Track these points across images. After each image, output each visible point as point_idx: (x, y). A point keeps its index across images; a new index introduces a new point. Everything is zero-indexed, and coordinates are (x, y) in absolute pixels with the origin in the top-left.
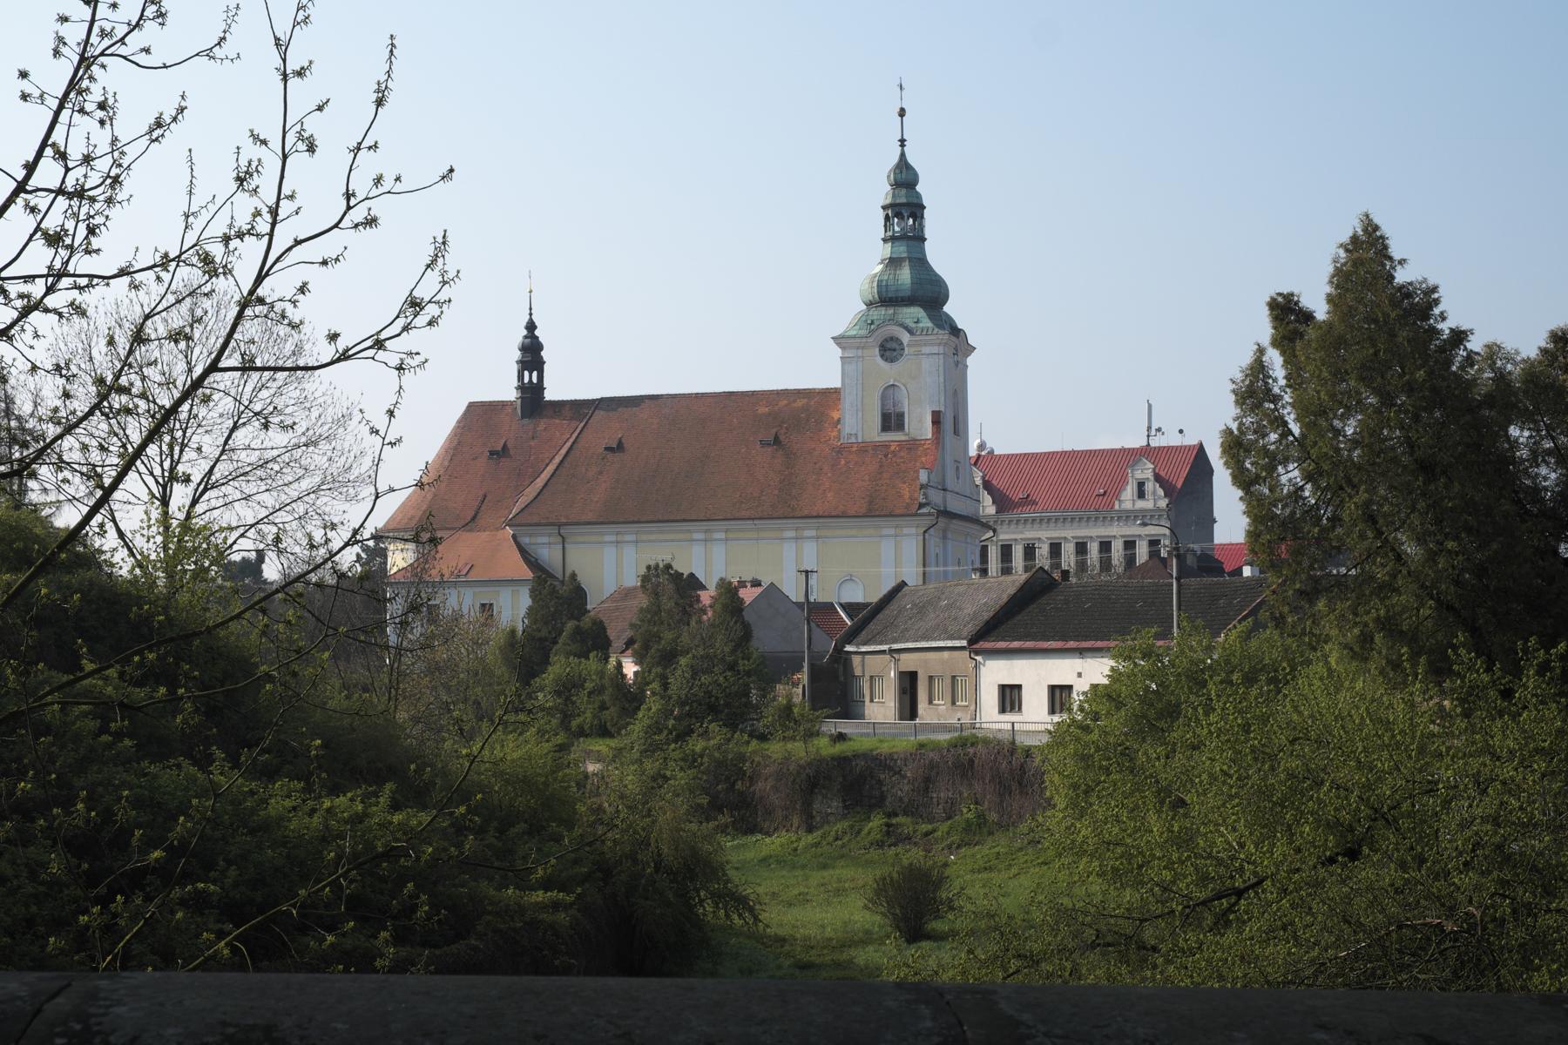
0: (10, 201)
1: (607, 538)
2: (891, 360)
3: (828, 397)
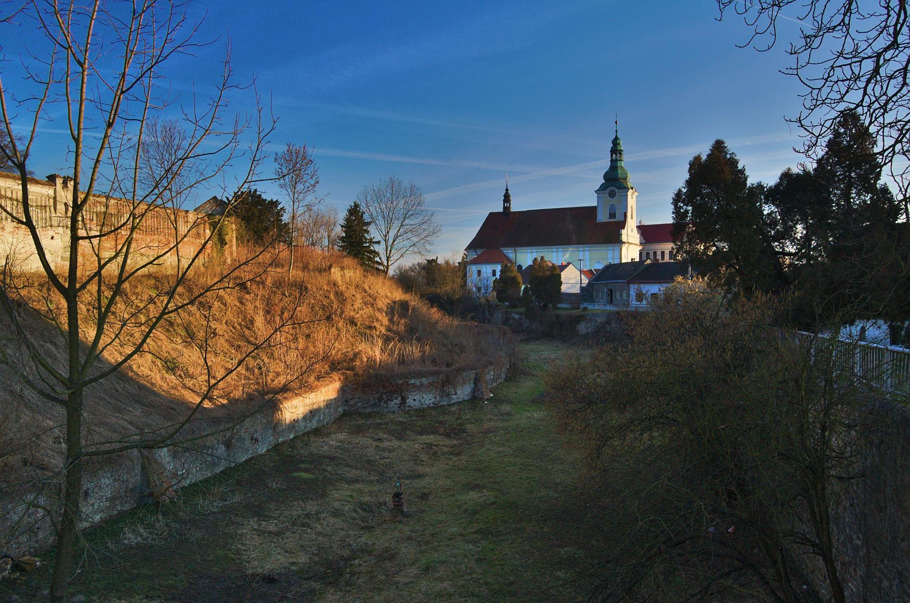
0: (907, 65)
1: (528, 251)
2: (611, 197)
3: (594, 209)
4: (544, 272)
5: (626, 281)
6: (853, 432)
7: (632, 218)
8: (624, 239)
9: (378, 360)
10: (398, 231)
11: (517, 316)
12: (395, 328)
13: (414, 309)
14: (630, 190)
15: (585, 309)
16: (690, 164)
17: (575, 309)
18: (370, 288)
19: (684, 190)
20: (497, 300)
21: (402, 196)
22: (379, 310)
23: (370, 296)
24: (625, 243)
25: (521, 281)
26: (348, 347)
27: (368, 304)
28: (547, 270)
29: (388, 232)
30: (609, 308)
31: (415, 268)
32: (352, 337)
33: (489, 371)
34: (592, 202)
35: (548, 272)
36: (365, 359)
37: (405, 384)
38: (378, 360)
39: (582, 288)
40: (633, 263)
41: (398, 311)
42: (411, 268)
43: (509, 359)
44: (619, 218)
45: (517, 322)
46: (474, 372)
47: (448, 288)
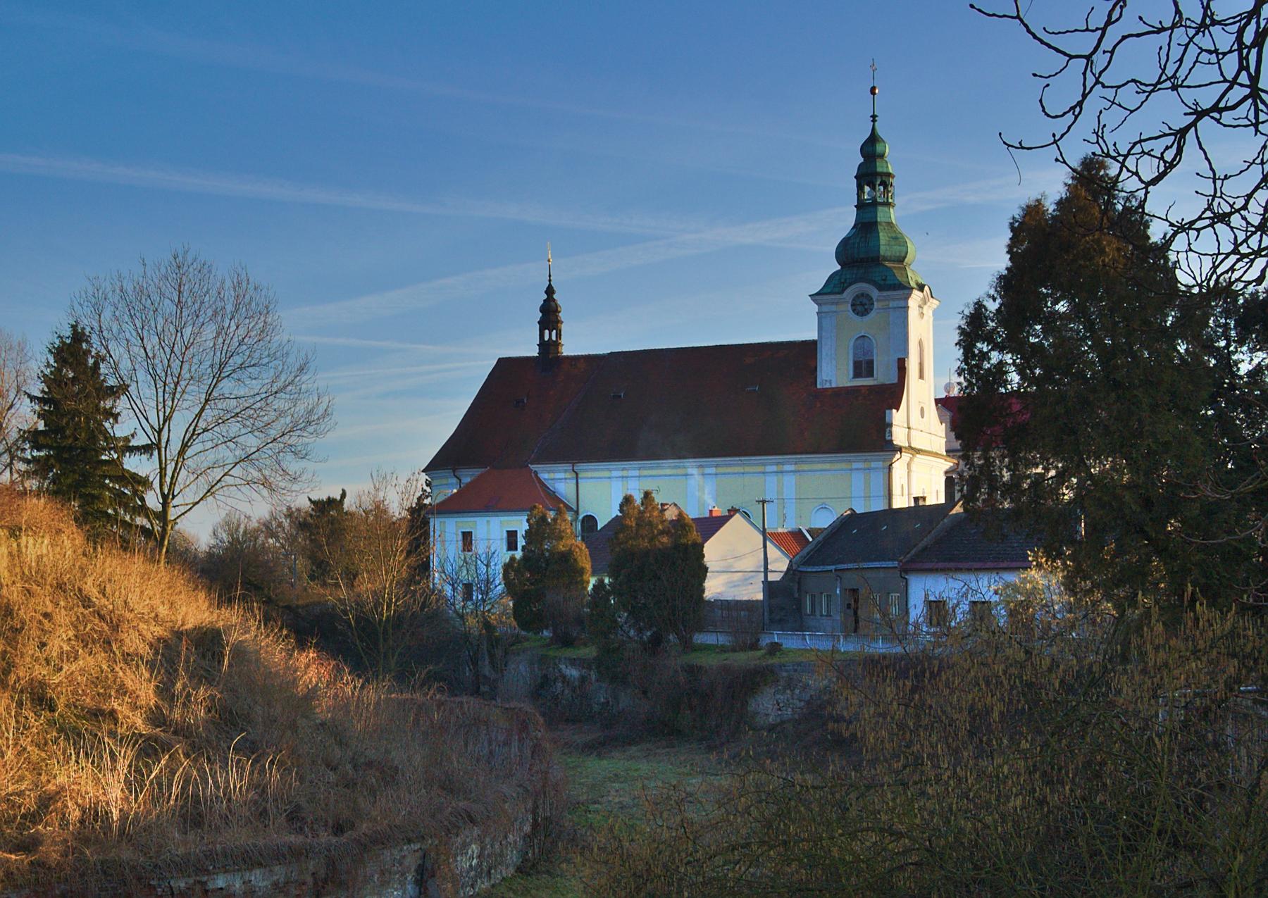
3: (807, 351)
4: (651, 540)
5: (896, 564)
7: (921, 376)
8: (899, 436)
9: (116, 815)
10: (199, 415)
11: (573, 673)
12: (177, 715)
13: (240, 652)
14: (916, 294)
15: (775, 648)
16: (1013, 229)
17: (743, 648)
18: (103, 592)
19: (992, 306)
20: (514, 623)
21: (210, 312)
22: (128, 658)
23: (102, 618)
24: (900, 449)
25: (588, 566)
26: (21, 779)
27: (94, 642)
28: (662, 533)
29: (167, 419)
30: (847, 646)
31: (280, 525)
32: (38, 745)
33: (465, 846)
34: (802, 327)
35: (665, 539)
36: (75, 815)
37: (198, 888)
38: (116, 815)
39: (769, 587)
40: (919, 510)
41: (187, 661)
42: (267, 525)
43: (530, 805)
44: (883, 375)
45: (574, 689)
46: (418, 846)
47: (365, 586)
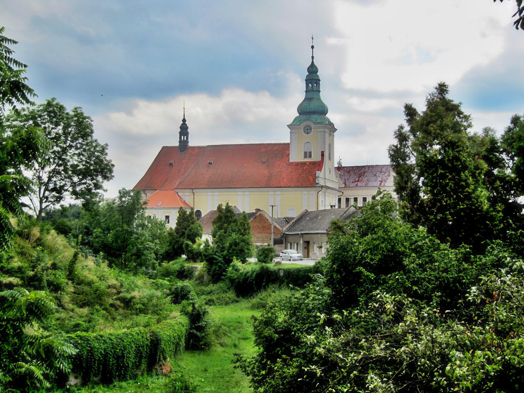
3: (286, 146)
6: (421, 228)
